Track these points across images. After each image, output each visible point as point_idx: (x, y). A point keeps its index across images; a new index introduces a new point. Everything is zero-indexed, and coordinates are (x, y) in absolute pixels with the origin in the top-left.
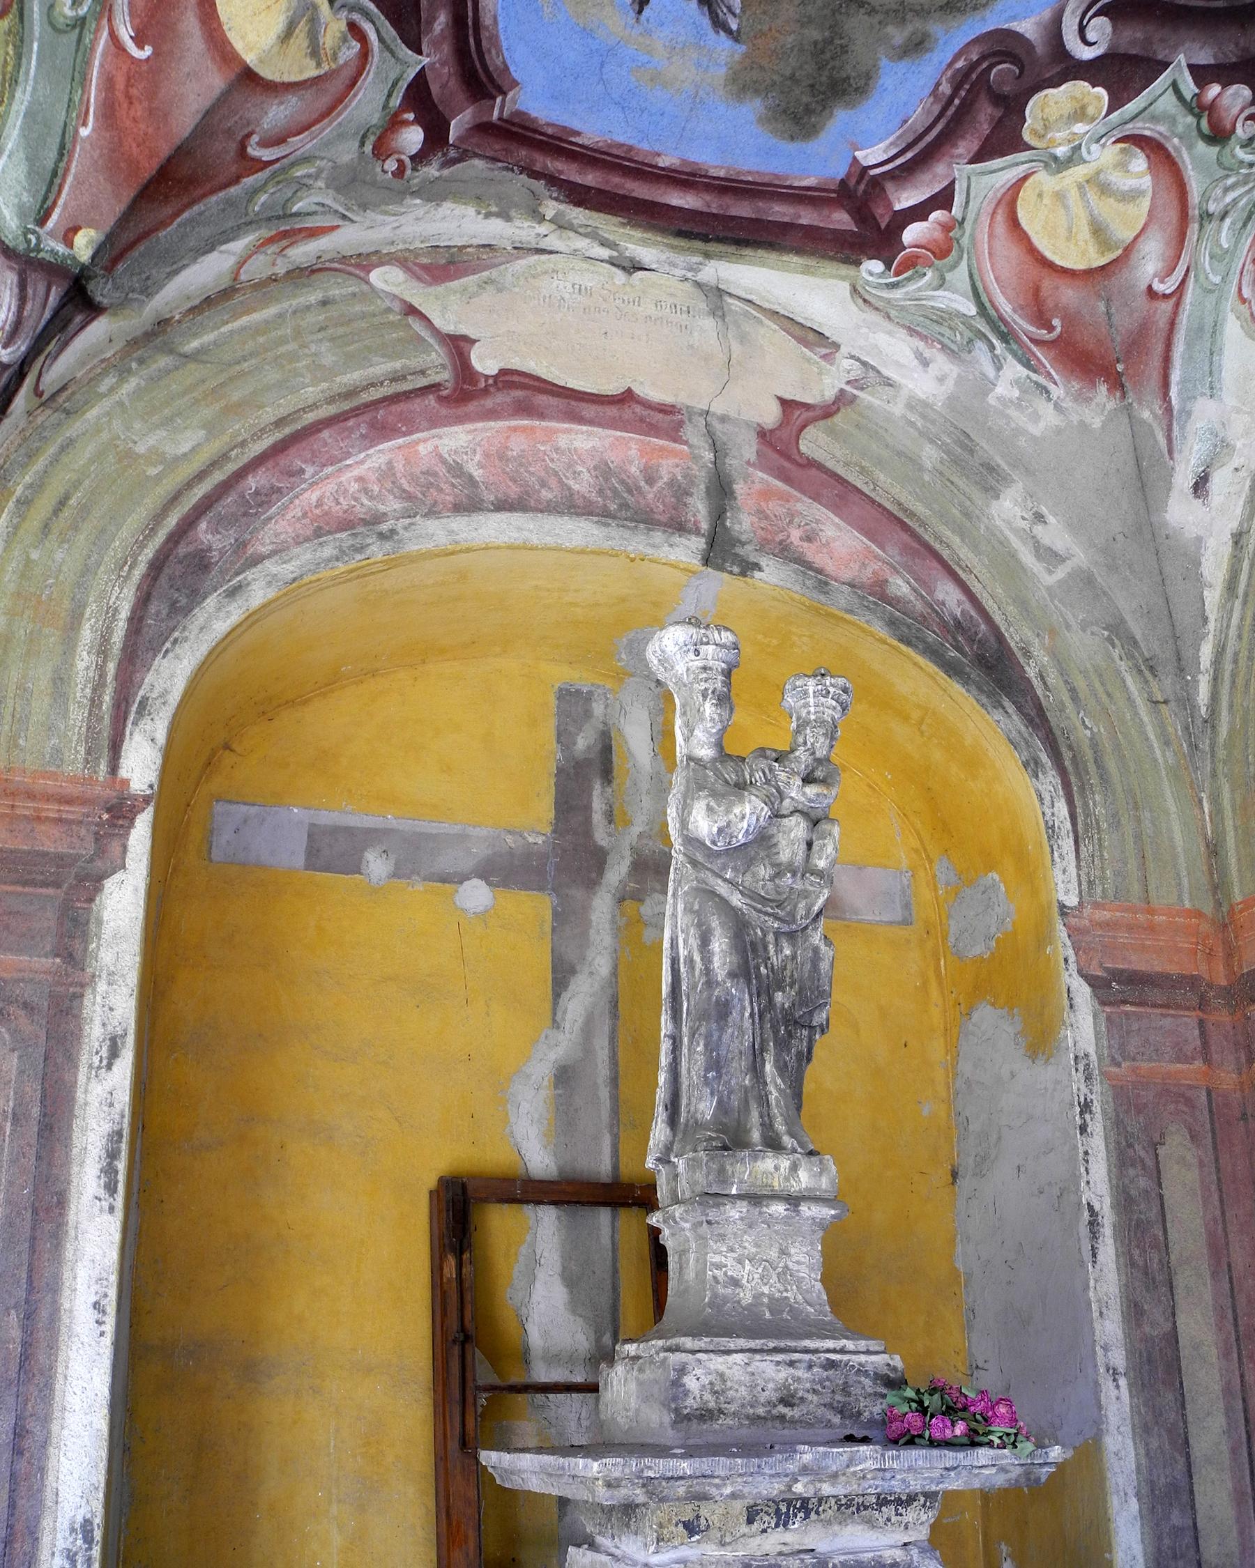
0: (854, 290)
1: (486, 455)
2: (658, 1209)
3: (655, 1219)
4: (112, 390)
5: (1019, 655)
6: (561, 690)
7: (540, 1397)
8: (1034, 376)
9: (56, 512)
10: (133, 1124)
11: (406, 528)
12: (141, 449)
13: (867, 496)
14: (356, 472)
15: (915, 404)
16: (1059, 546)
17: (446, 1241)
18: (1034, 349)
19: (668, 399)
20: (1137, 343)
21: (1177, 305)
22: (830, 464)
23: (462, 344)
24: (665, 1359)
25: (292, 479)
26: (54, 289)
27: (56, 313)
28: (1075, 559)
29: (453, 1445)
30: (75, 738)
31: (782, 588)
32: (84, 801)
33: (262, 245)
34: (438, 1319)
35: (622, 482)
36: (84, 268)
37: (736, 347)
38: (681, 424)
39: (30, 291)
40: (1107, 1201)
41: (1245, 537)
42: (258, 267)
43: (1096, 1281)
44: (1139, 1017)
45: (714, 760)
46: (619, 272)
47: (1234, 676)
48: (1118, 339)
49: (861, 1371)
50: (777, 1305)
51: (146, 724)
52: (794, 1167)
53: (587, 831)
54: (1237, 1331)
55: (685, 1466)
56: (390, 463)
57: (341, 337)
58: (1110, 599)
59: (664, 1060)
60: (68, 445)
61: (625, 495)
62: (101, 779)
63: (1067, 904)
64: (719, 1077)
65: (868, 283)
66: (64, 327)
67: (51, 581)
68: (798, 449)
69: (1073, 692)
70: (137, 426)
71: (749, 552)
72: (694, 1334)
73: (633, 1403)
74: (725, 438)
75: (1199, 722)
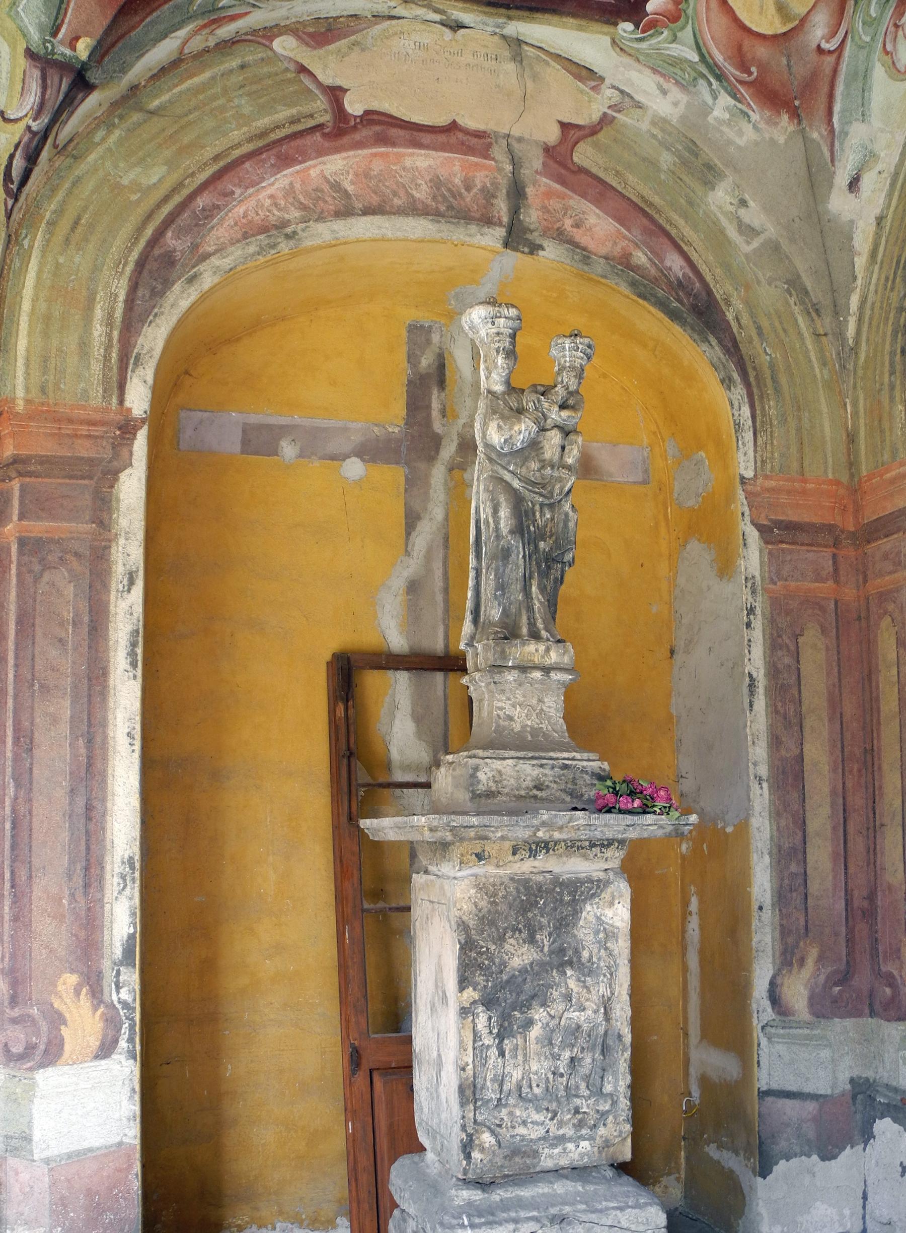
0: (614, 42)
1: (356, 175)
2: (467, 674)
3: (465, 680)
4: (103, 139)
5: (722, 304)
6: (410, 325)
7: (398, 791)
8: (739, 105)
9: (73, 229)
10: (145, 626)
11: (303, 230)
12: (125, 181)
13: (620, 193)
14: (269, 191)
15: (660, 122)
16: (756, 223)
17: (338, 694)
18: (739, 87)
19: (481, 127)
20: (809, 85)
21: (839, 58)
22: (594, 170)
23: (338, 93)
24: (467, 762)
25: (226, 199)
26: (64, 80)
27: (67, 95)
28: (767, 233)
29: (344, 819)
30: (96, 382)
31: (558, 262)
32: (103, 423)
33: (199, 30)
34: (333, 742)
35: (449, 190)
36: (84, 64)
37: (530, 84)
38: (490, 145)
39: (49, 82)
40: (762, 671)
41: (884, 220)
42: (197, 44)
43: (751, 722)
44: (791, 552)
45: (504, 393)
46: (447, 31)
47: (871, 319)
48: (796, 83)
49: (584, 771)
50: (535, 732)
51: (140, 371)
52: (548, 650)
53: (428, 421)
54: (843, 756)
55: (474, 820)
56: (291, 183)
57: (255, 92)
58: (790, 261)
59: (471, 583)
60: (77, 182)
61: (451, 199)
62: (114, 408)
63: (746, 476)
64: (504, 594)
65: (623, 37)
66: (72, 102)
67: (73, 277)
68: (572, 159)
69: (759, 329)
70: (122, 165)
71: (535, 237)
72: (484, 748)
73: (450, 789)
74: (520, 154)
75: (847, 349)
